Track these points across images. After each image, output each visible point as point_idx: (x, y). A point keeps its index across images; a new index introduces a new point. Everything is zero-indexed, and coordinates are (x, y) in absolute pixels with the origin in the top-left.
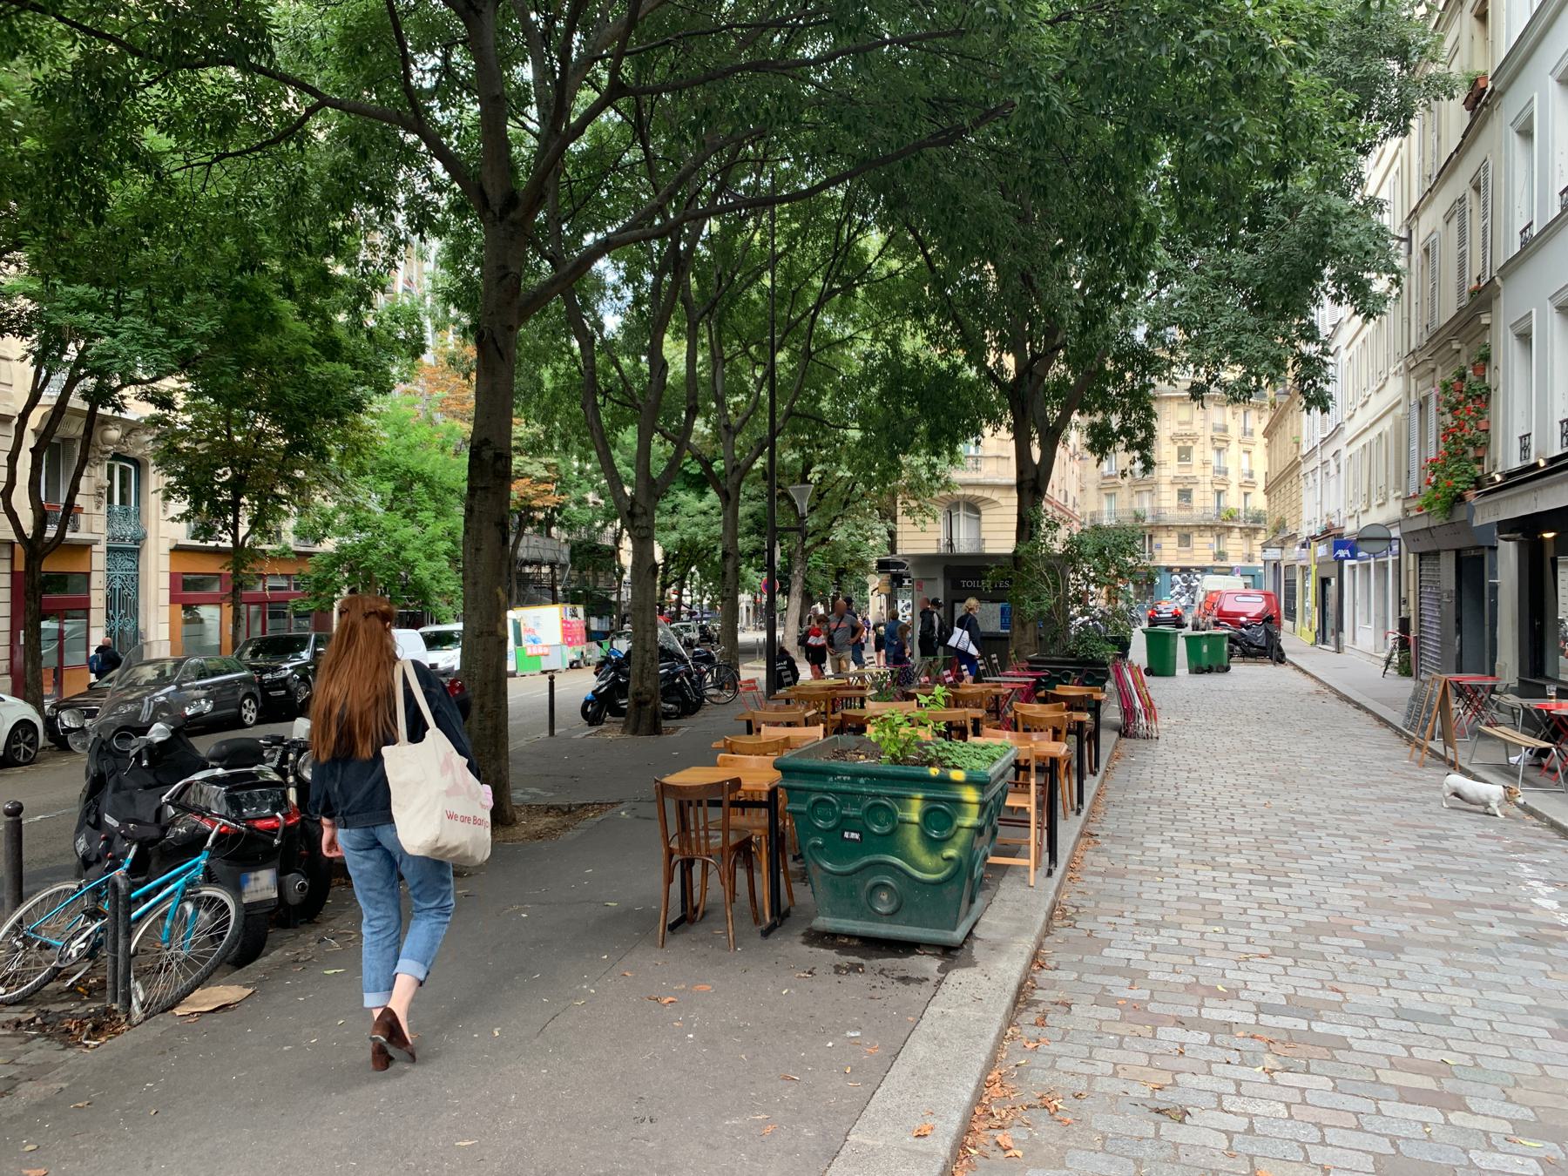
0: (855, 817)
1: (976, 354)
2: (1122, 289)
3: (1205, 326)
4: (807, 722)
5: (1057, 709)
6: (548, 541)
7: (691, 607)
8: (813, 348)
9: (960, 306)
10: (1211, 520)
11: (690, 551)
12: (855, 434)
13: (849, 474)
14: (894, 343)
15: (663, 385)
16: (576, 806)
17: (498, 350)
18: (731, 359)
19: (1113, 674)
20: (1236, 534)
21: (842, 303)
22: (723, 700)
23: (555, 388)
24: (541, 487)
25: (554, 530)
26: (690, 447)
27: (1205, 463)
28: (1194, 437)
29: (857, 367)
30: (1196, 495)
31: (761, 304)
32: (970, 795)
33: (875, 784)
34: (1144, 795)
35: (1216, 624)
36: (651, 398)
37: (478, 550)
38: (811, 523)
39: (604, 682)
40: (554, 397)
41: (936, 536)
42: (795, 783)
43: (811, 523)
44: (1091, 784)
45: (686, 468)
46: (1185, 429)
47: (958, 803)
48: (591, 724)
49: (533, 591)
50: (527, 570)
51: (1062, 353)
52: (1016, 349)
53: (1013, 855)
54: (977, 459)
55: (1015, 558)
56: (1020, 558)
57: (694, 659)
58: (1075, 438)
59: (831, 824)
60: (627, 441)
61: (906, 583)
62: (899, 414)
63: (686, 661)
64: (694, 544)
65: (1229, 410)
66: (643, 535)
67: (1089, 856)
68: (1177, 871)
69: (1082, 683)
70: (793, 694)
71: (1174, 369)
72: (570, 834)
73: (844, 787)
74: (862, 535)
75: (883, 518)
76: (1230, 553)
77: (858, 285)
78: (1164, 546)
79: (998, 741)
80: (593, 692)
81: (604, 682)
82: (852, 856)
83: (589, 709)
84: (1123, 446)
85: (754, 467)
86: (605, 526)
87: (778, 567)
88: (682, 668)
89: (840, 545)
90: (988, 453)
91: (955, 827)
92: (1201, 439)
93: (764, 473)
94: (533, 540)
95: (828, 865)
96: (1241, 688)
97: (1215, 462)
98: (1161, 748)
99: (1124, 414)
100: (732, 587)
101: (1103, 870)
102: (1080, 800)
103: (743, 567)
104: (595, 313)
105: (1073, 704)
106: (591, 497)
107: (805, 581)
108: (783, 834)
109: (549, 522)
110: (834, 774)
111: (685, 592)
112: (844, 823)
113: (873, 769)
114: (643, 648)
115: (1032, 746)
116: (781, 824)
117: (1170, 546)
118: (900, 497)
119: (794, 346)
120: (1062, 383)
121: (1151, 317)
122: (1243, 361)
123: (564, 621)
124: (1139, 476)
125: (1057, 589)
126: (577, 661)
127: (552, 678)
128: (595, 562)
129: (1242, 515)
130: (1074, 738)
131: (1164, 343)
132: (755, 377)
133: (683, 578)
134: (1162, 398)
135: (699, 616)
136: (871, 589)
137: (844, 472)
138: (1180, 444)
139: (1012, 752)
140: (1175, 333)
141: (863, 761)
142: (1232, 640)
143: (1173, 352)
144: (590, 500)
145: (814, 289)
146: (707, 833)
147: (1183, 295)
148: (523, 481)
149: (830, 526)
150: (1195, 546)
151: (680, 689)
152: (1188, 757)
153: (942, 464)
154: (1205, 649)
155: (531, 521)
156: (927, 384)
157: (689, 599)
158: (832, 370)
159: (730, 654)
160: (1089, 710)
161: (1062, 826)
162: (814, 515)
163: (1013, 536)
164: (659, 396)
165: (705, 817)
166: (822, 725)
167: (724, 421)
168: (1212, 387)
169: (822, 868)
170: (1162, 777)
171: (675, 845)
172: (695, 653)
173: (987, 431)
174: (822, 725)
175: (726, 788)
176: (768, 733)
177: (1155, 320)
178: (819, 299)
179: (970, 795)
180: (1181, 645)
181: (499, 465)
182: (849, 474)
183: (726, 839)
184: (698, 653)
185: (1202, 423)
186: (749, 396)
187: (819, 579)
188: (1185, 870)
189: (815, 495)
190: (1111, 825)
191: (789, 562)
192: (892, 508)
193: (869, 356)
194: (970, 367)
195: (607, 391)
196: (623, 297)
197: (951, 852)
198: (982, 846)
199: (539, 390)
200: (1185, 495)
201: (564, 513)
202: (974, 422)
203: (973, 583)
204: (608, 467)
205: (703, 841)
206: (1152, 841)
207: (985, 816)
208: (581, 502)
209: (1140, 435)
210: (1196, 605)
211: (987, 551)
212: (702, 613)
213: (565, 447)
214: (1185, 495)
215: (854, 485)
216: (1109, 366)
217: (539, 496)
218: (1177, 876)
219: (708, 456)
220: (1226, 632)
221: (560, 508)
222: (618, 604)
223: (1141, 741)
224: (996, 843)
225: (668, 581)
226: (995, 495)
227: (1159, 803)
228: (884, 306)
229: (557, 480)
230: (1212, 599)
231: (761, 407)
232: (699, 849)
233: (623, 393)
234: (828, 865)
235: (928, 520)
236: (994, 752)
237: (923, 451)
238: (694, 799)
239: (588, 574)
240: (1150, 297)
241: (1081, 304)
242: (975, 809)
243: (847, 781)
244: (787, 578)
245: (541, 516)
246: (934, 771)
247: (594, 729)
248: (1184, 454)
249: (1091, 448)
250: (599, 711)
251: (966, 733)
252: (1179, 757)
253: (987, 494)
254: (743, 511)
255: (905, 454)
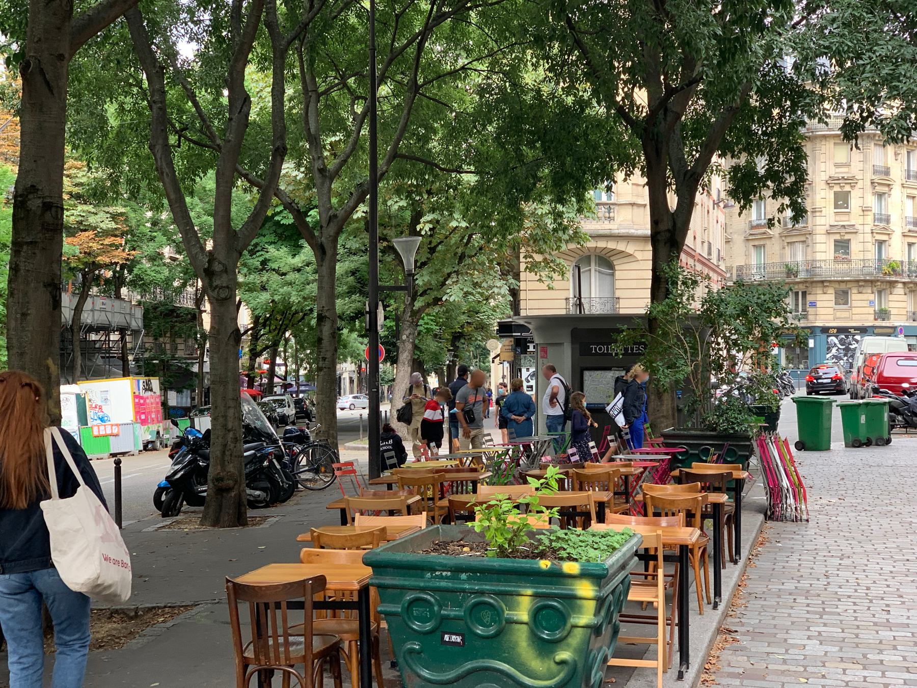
0: (457, 618)
1: (604, 91)
2: (764, 14)
3: (859, 56)
4: (410, 510)
5: (692, 490)
6: (117, 303)
7: (285, 379)
8: (421, 81)
9: (585, 33)
10: (871, 274)
11: (283, 313)
12: (470, 179)
13: (464, 224)
14: (513, 74)
15: (244, 122)
16: (144, 609)
17: (47, 83)
18: (326, 92)
19: (757, 449)
20: (899, 290)
21: (453, 29)
22: (320, 485)
23: (121, 126)
24: (107, 241)
25: (124, 291)
26: (278, 193)
27: (865, 210)
28: (851, 181)
29: (471, 101)
30: (855, 247)
31: (361, 30)
32: (585, 589)
33: (479, 579)
34: (790, 586)
35: (876, 391)
36: (231, 137)
37: (24, 315)
38: (422, 279)
39: (179, 466)
40: (120, 135)
41: (564, 295)
42: (388, 581)
43: (422, 279)
44: (731, 574)
45: (276, 218)
46: (843, 172)
47: (572, 599)
48: (165, 515)
49: (99, 361)
50: (93, 337)
51: (701, 87)
52: (649, 82)
53: (639, 656)
54: (609, 206)
55: (650, 321)
56: (655, 319)
57: (286, 439)
58: (718, 184)
59: (428, 626)
60: (208, 187)
61: (531, 349)
62: (520, 156)
63: (275, 442)
64: (288, 306)
65: (890, 149)
66: (223, 296)
67: (726, 655)
68: (824, 671)
69: (721, 459)
70: (395, 477)
71: (826, 105)
72: (135, 643)
73: (443, 584)
74: (482, 294)
75: (504, 274)
76: (893, 311)
77: (470, 8)
78: (819, 304)
79: (619, 528)
80: (167, 478)
81: (179, 466)
82: (453, 662)
83: (163, 498)
84: (770, 193)
85: (355, 217)
86: (184, 285)
87: (382, 332)
88: (270, 450)
89: (456, 306)
90: (622, 201)
91: (568, 626)
92: (860, 183)
93: (367, 223)
94: (99, 302)
95: (425, 673)
96: (903, 463)
97: (875, 210)
98: (812, 532)
99: (771, 156)
100: (328, 355)
101: (741, 671)
102: (718, 593)
103: (345, 331)
104: (166, 40)
105: (711, 484)
106: (167, 251)
107: (416, 347)
108: (377, 638)
109: (118, 281)
110: (433, 570)
111: (279, 361)
112: (444, 624)
113: (475, 562)
114: (225, 426)
115: (660, 532)
116: (373, 626)
117: (826, 304)
118: (523, 250)
119: (399, 77)
120: (699, 121)
121: (798, 44)
122: (904, 96)
123: (136, 396)
124: (790, 226)
125: (694, 354)
126: (152, 442)
127: (118, 463)
128: (172, 327)
129: (906, 269)
130: (709, 523)
131: (813, 74)
132: (355, 113)
133: (276, 344)
134: (816, 137)
135: (295, 388)
136: (492, 355)
137: (458, 222)
138: (837, 189)
139: (635, 540)
140: (826, 64)
141: (467, 555)
142: (893, 409)
143: (823, 85)
144: (167, 255)
145: (421, 12)
146: (286, 640)
147: (834, 20)
148: (87, 234)
149: (443, 284)
150: (854, 304)
151: (269, 473)
152: (841, 541)
153: (569, 212)
154: (863, 419)
155: (97, 280)
156: (551, 122)
157: (283, 368)
158: (442, 105)
159: (327, 432)
160: (728, 490)
161: (694, 621)
162: (425, 271)
163: (648, 293)
164: (241, 134)
165: (285, 621)
166: (424, 513)
167: (318, 165)
168: (867, 124)
169: (419, 676)
170: (811, 564)
171: (250, 654)
172: (286, 432)
173: (620, 176)
174: (424, 513)
175: (309, 588)
176: (364, 523)
177: (804, 49)
178: (427, 24)
179: (585, 589)
180: (836, 416)
181: (48, 216)
182: (464, 224)
183: (309, 645)
184: (290, 431)
185: (861, 165)
186: (348, 136)
187: (431, 345)
188: (833, 668)
189: (426, 249)
190: (751, 620)
191: (397, 325)
192: (515, 262)
193: (482, 91)
194: (599, 103)
195: (182, 130)
196: (200, 21)
197: (564, 655)
198: (602, 647)
199: (102, 128)
200: (842, 246)
201: (136, 271)
202: (603, 166)
203: (604, 348)
204: (182, 216)
205: (282, 649)
206: (797, 637)
207: (603, 613)
208: (156, 258)
209: (790, 180)
210: (855, 370)
211: (622, 312)
212: (298, 385)
213: (134, 195)
214: (842, 246)
215: (470, 236)
216: (754, 102)
217: (105, 250)
218: (824, 676)
219: (302, 203)
220: (887, 400)
221: (130, 265)
222: (200, 375)
223: (789, 524)
224: (619, 643)
225: (259, 348)
226: (630, 248)
227: (807, 594)
228: (501, 33)
229: (127, 233)
230: (872, 362)
231: (362, 148)
232: (277, 658)
233: (201, 131)
234: (425, 673)
235: (555, 276)
236: (614, 541)
237: (547, 198)
238: (272, 601)
239: (165, 340)
240: (798, 23)
241: (720, 32)
242: (591, 606)
243: (447, 577)
244: (394, 345)
245: (109, 274)
246: (544, 564)
247: (168, 521)
248: (842, 200)
249: (733, 193)
250: (175, 498)
251: (590, 519)
252: (830, 542)
253: (621, 246)
254: (340, 268)
255: (527, 200)
